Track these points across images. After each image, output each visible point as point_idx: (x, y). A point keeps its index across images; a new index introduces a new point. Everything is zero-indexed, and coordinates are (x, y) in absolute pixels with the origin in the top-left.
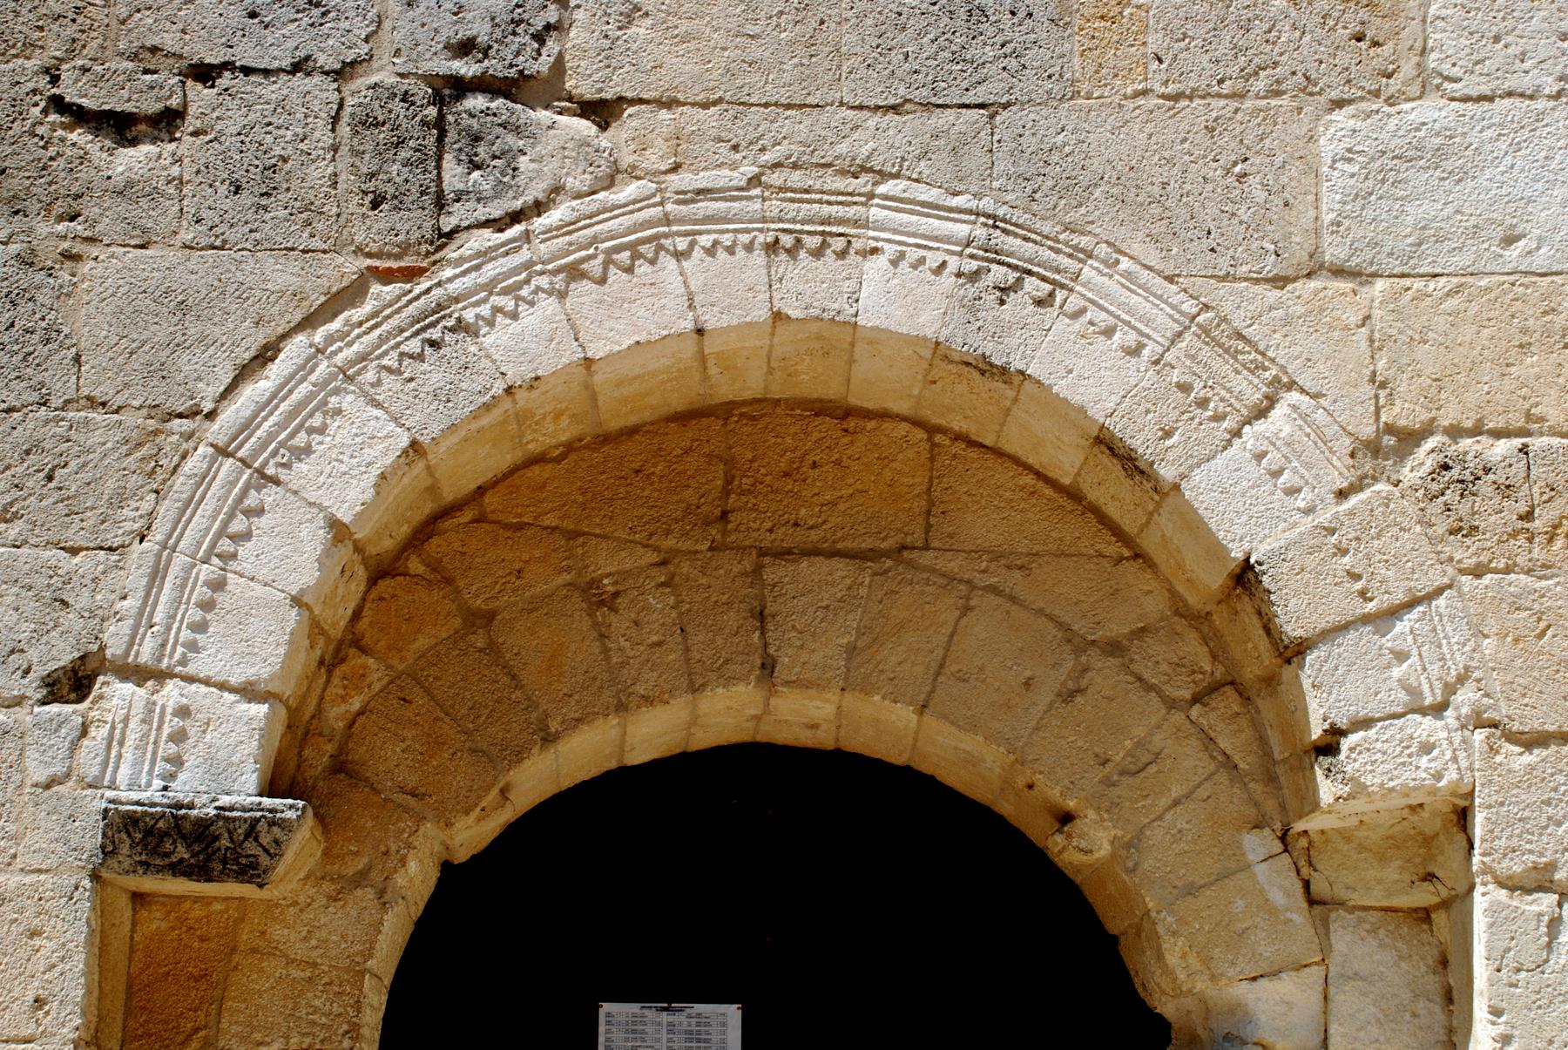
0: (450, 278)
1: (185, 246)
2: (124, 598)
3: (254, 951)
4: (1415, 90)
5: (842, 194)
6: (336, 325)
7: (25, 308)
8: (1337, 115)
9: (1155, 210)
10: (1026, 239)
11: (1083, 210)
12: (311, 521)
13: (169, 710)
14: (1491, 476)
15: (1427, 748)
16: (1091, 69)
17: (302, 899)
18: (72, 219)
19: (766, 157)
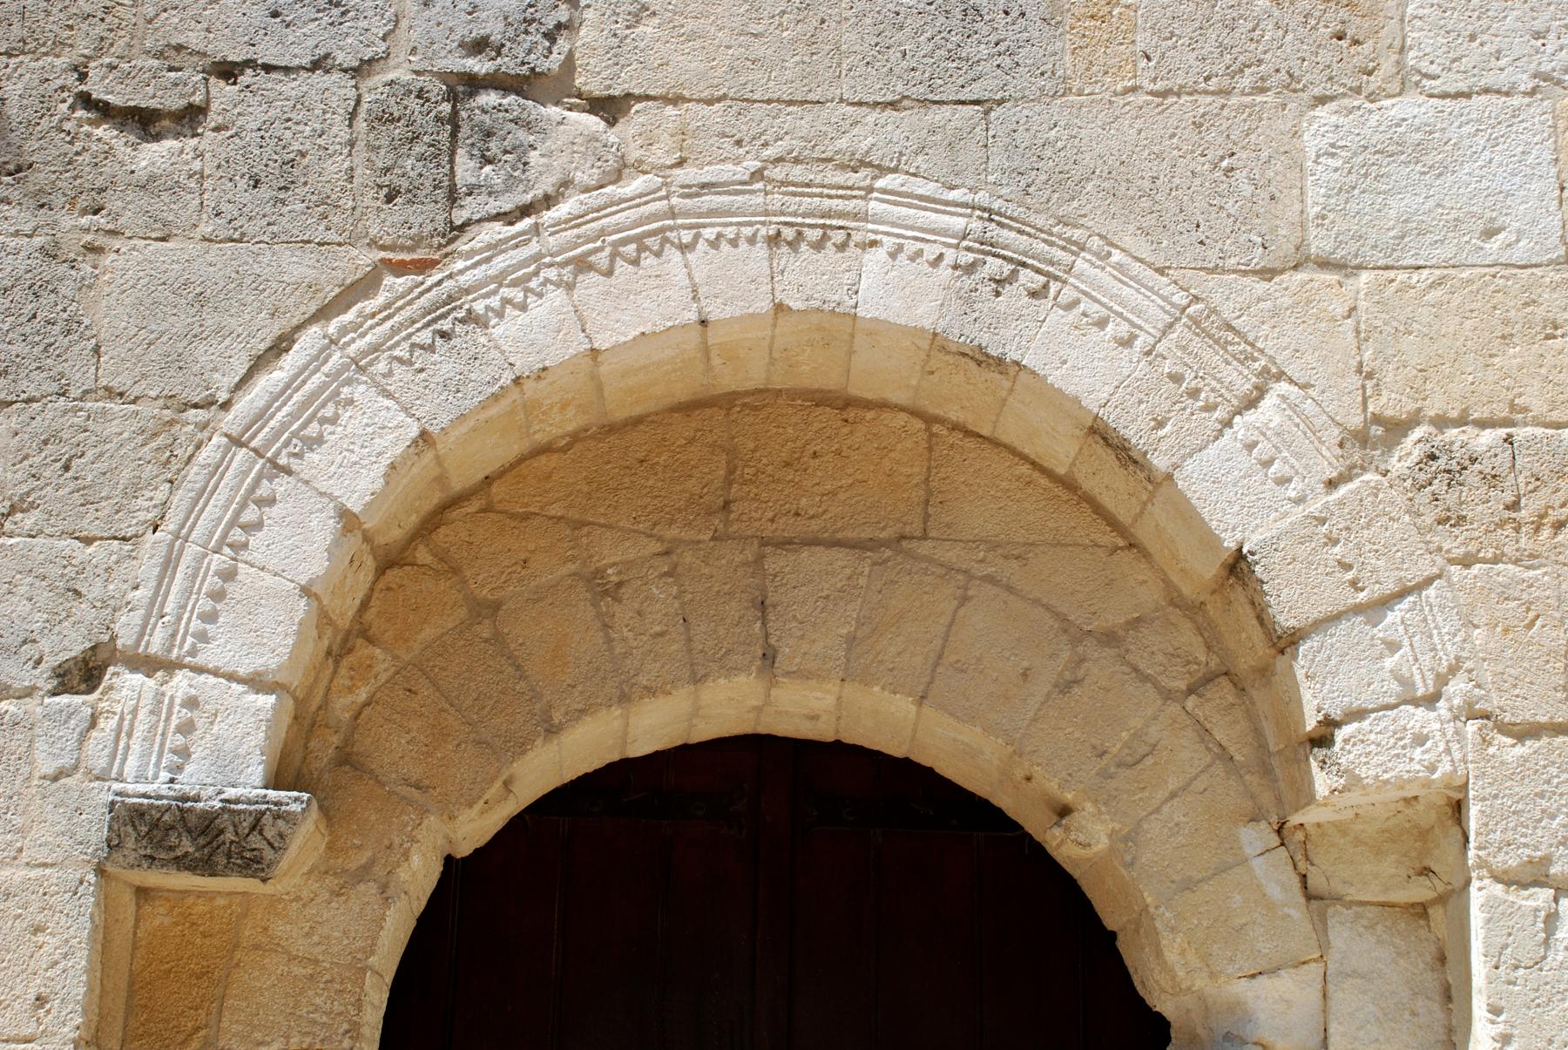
0: (462, 270)
1: (205, 239)
2: (136, 588)
3: (257, 947)
4: (1394, 87)
5: (842, 188)
6: (350, 316)
7: (47, 299)
8: (1321, 112)
9: (1145, 203)
10: (1020, 232)
11: (1075, 204)
12: (321, 511)
13: (178, 701)
14: (1477, 466)
15: (1420, 740)
16: (1082, 67)
17: (305, 894)
18: (96, 212)
19: (769, 152)
